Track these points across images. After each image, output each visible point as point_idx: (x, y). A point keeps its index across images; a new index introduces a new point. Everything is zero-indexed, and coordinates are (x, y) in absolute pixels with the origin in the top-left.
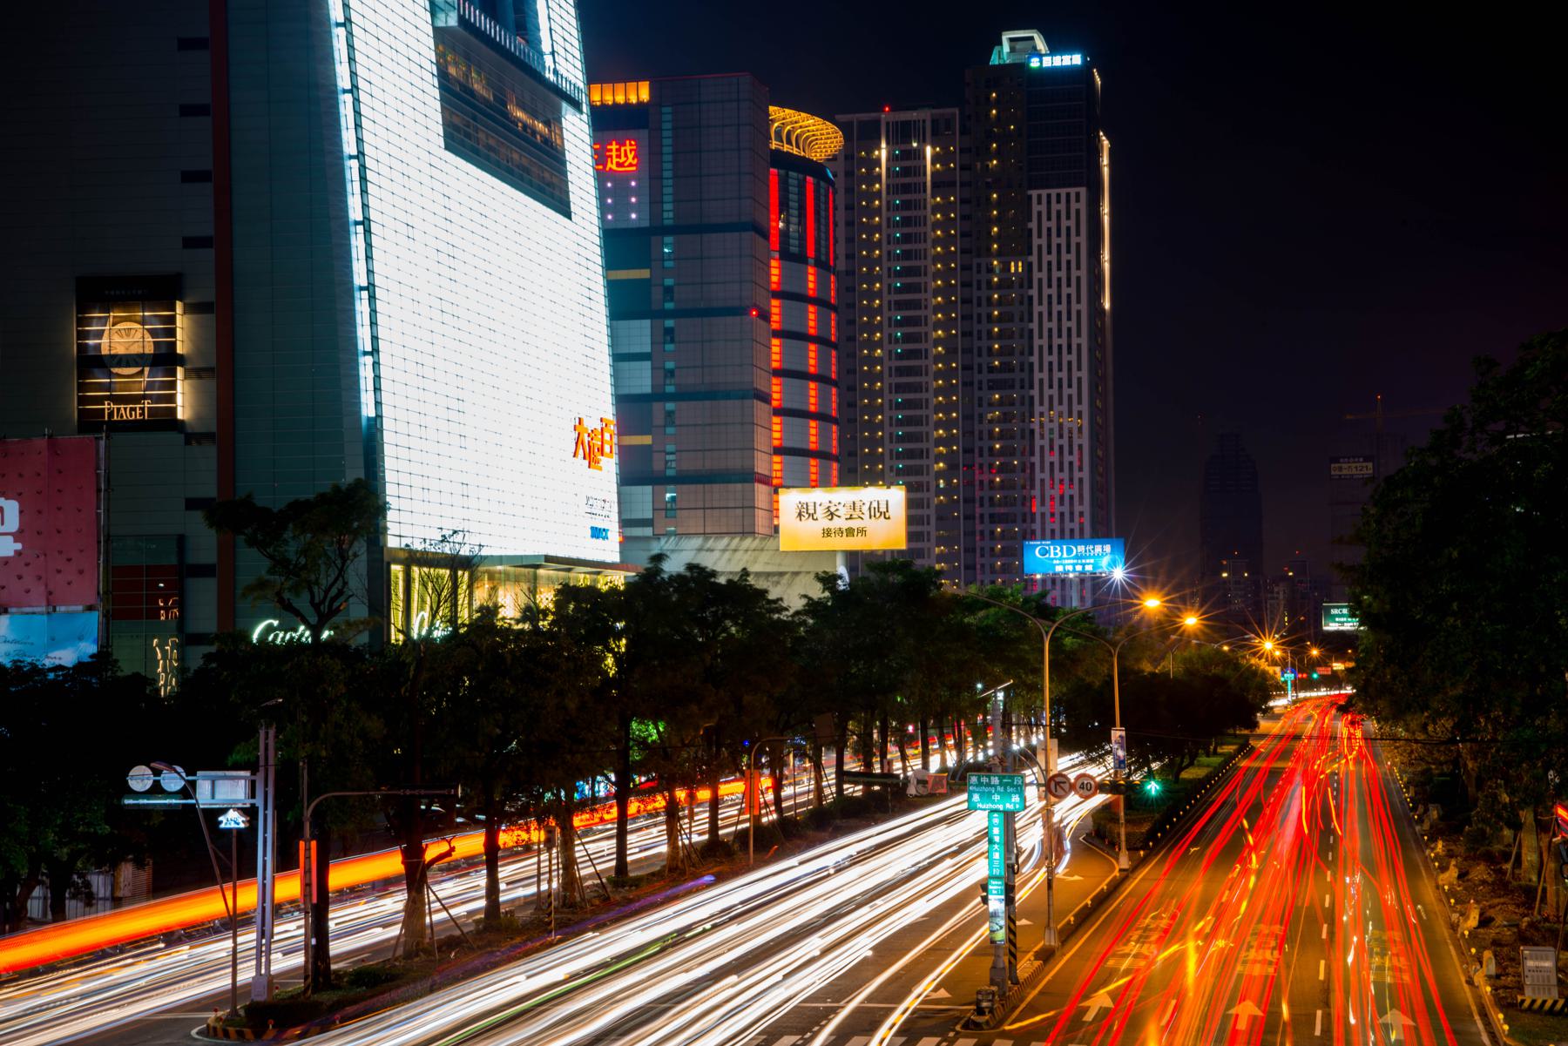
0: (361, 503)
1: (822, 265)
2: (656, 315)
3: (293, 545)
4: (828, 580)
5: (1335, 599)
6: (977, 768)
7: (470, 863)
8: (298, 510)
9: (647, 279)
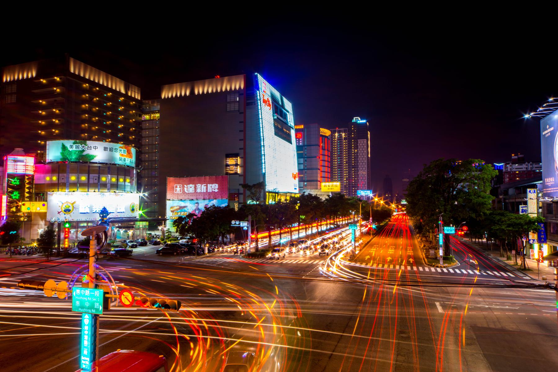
0: (261, 185)
1: (328, 150)
2: (304, 158)
3: (253, 190)
4: (329, 196)
5: (404, 199)
6: (350, 223)
7: (278, 234)
8: (254, 185)
9: (303, 153)
